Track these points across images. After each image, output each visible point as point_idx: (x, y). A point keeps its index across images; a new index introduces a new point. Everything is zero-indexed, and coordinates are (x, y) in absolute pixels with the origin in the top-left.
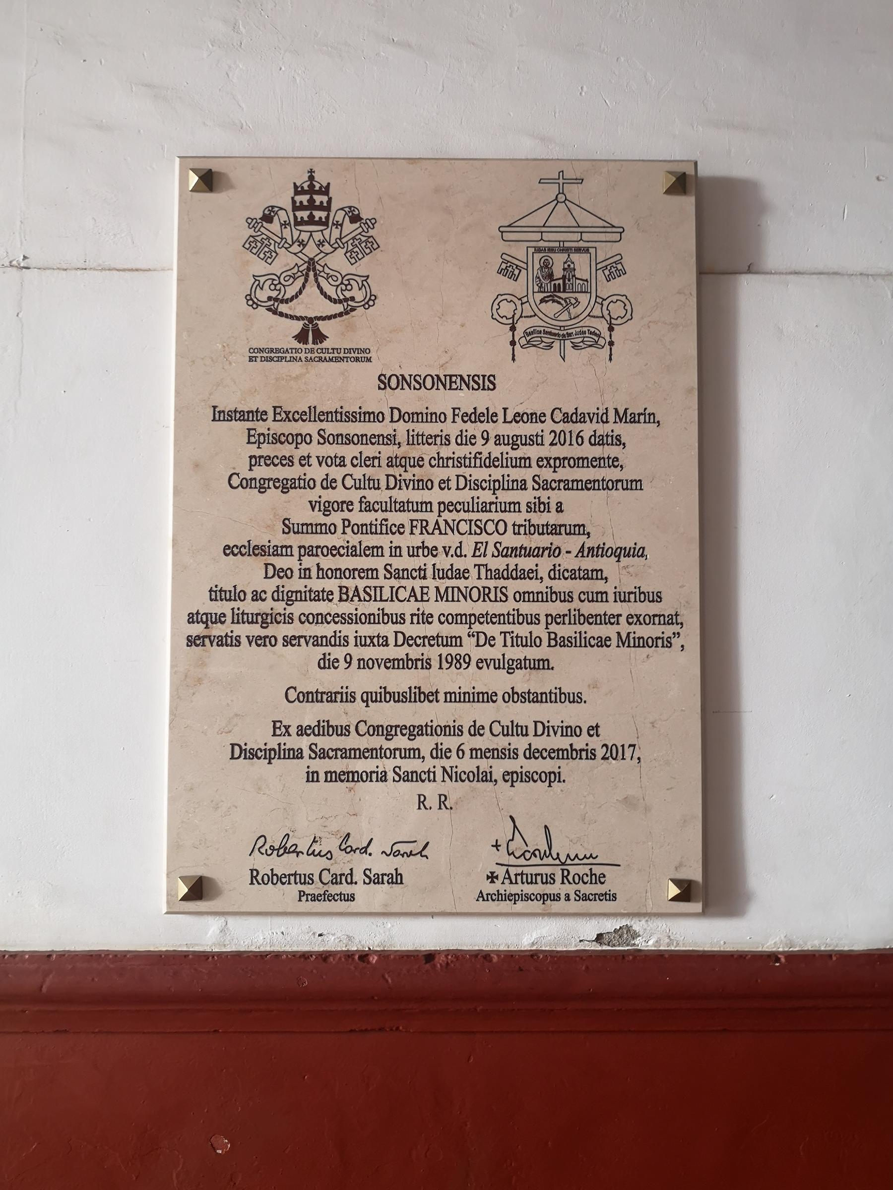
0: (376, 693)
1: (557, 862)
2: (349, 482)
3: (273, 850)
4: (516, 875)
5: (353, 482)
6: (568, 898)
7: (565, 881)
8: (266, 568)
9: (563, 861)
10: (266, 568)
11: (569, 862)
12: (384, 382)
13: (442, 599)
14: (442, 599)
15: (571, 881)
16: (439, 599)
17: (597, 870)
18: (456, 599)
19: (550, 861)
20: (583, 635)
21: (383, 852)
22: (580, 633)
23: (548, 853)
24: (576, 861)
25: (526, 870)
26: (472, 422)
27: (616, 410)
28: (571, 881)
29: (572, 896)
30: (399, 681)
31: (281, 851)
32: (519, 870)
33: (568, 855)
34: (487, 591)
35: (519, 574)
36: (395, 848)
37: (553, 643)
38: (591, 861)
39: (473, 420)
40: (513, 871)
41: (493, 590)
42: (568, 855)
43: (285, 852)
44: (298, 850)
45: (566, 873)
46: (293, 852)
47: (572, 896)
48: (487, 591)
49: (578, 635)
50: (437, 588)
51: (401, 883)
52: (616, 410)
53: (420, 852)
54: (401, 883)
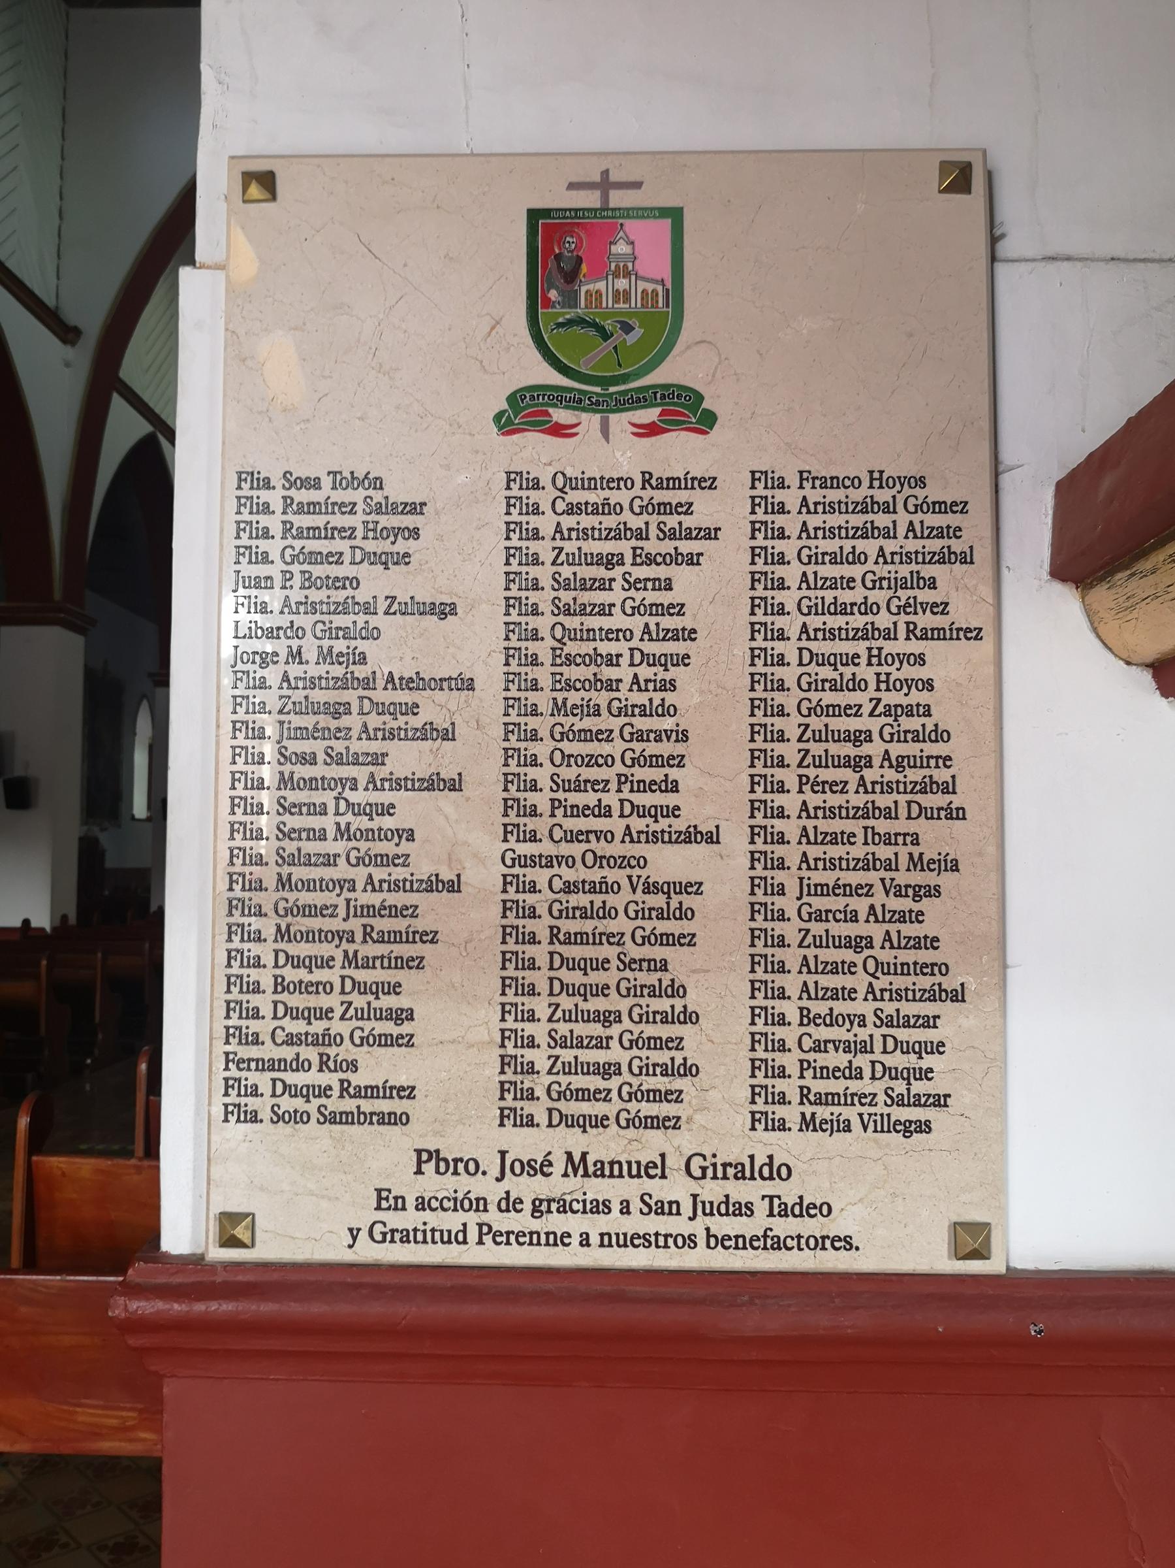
0: (915, 757)
2: (558, 834)
5: (562, 834)
6: (626, 1209)
8: (622, 804)
10: (622, 804)
12: (425, 1157)
13: (915, 866)
14: (915, 866)
16: (912, 867)
26: (826, 1025)
27: (569, 1155)
29: (636, 1205)
35: (854, 1073)
39: (828, 1022)
47: (636, 1205)
50: (911, 854)
51: (964, 818)
52: (569, 1155)
54: (964, 818)
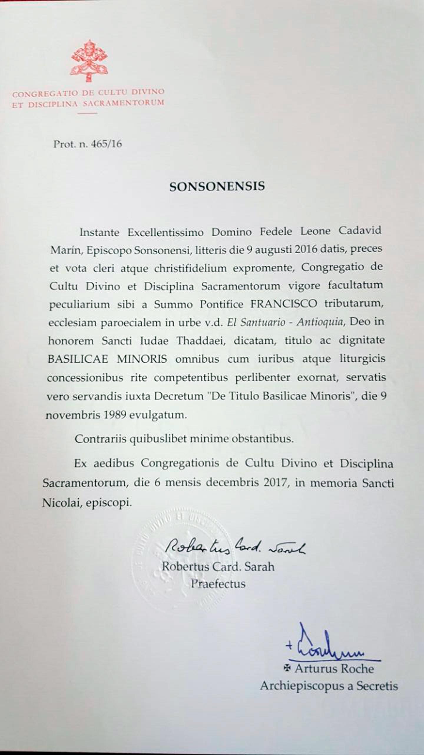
1: (334, 658)
3: (184, 548)
4: (306, 668)
7: (344, 671)
9: (339, 657)
11: (343, 658)
15: (348, 671)
17: (368, 665)
18: (131, 361)
19: (328, 657)
20: (287, 394)
21: (270, 550)
22: (285, 392)
23: (327, 651)
24: (348, 657)
25: (313, 664)
28: (348, 671)
30: (158, 428)
31: (190, 549)
32: (308, 665)
33: (343, 654)
34: (154, 357)
36: (279, 547)
37: (266, 397)
38: (359, 657)
40: (303, 665)
41: (157, 357)
42: (343, 654)
43: (193, 549)
44: (203, 548)
45: (345, 666)
46: (200, 549)
48: (154, 357)
49: (283, 394)
53: (300, 550)
